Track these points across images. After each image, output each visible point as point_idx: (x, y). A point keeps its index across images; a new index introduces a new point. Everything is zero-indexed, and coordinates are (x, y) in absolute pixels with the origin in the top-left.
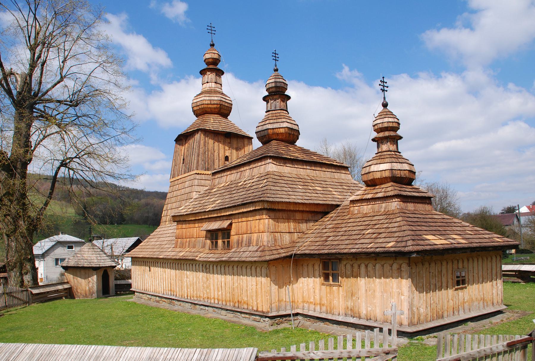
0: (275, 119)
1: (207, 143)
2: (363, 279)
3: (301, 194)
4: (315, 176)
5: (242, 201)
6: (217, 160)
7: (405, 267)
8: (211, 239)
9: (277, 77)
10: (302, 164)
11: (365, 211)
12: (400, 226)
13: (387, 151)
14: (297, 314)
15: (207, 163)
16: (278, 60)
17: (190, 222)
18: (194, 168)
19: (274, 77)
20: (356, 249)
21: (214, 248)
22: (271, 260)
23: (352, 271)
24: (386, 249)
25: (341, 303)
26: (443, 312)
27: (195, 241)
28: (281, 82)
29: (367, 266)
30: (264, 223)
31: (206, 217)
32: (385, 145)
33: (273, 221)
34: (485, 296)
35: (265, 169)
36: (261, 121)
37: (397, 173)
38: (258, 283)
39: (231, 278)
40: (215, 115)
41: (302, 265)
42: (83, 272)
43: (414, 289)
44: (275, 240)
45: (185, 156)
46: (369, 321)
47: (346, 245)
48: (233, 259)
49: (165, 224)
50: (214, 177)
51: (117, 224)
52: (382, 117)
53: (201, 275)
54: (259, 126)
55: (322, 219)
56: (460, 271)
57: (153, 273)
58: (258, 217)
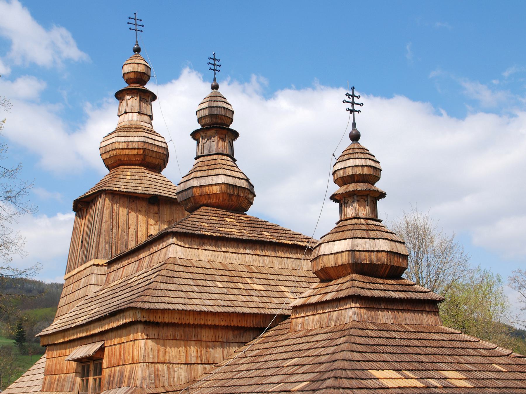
0: (205, 170)
1: (115, 214)
9: (214, 99)
10: (236, 245)
28: (220, 107)
31: (75, 337)
32: (351, 208)
33: (154, 344)
37: (362, 256)
40: (136, 167)
44: (157, 377)
45: (84, 236)
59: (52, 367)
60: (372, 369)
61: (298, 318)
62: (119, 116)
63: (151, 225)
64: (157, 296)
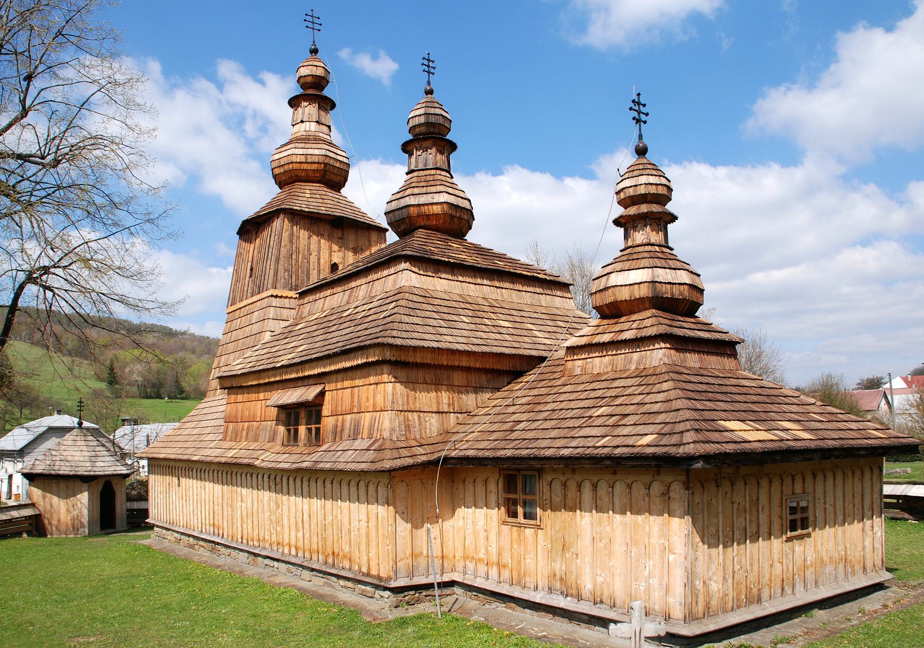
0: (423, 187)
1: (295, 238)
2: (587, 514)
3: (465, 333)
4: (500, 299)
5: (343, 346)
6: (316, 271)
7: (677, 490)
8: (287, 424)
11: (597, 368)
12: (668, 401)
13: (644, 245)
14: (452, 583)
15: (294, 276)
17: (250, 389)
18: (270, 286)
19: (424, 105)
20: (571, 450)
22: (395, 470)
23: (565, 496)
24: (636, 450)
25: (540, 564)
26: (759, 590)
28: (438, 115)
29: (596, 487)
30: (385, 391)
31: (278, 379)
32: (641, 232)
33: (403, 387)
34: (849, 553)
35: (395, 282)
36: (397, 190)
37: (664, 289)
38: (370, 516)
40: (315, 185)
41: (464, 482)
42: (62, 485)
43: (698, 539)
44: (408, 427)
45: (254, 263)
46: (598, 605)
47: (551, 440)
48: (321, 466)
49: (215, 395)
50: (301, 301)
51: (169, 399)
52: (635, 173)
53: (266, 496)
54: (391, 201)
55: (510, 386)
56: (797, 500)
57: (184, 490)
58: (372, 379)
59: (236, 413)
60: (720, 420)
61: (576, 360)
62: (293, 125)
63: (335, 252)
64: (405, 331)
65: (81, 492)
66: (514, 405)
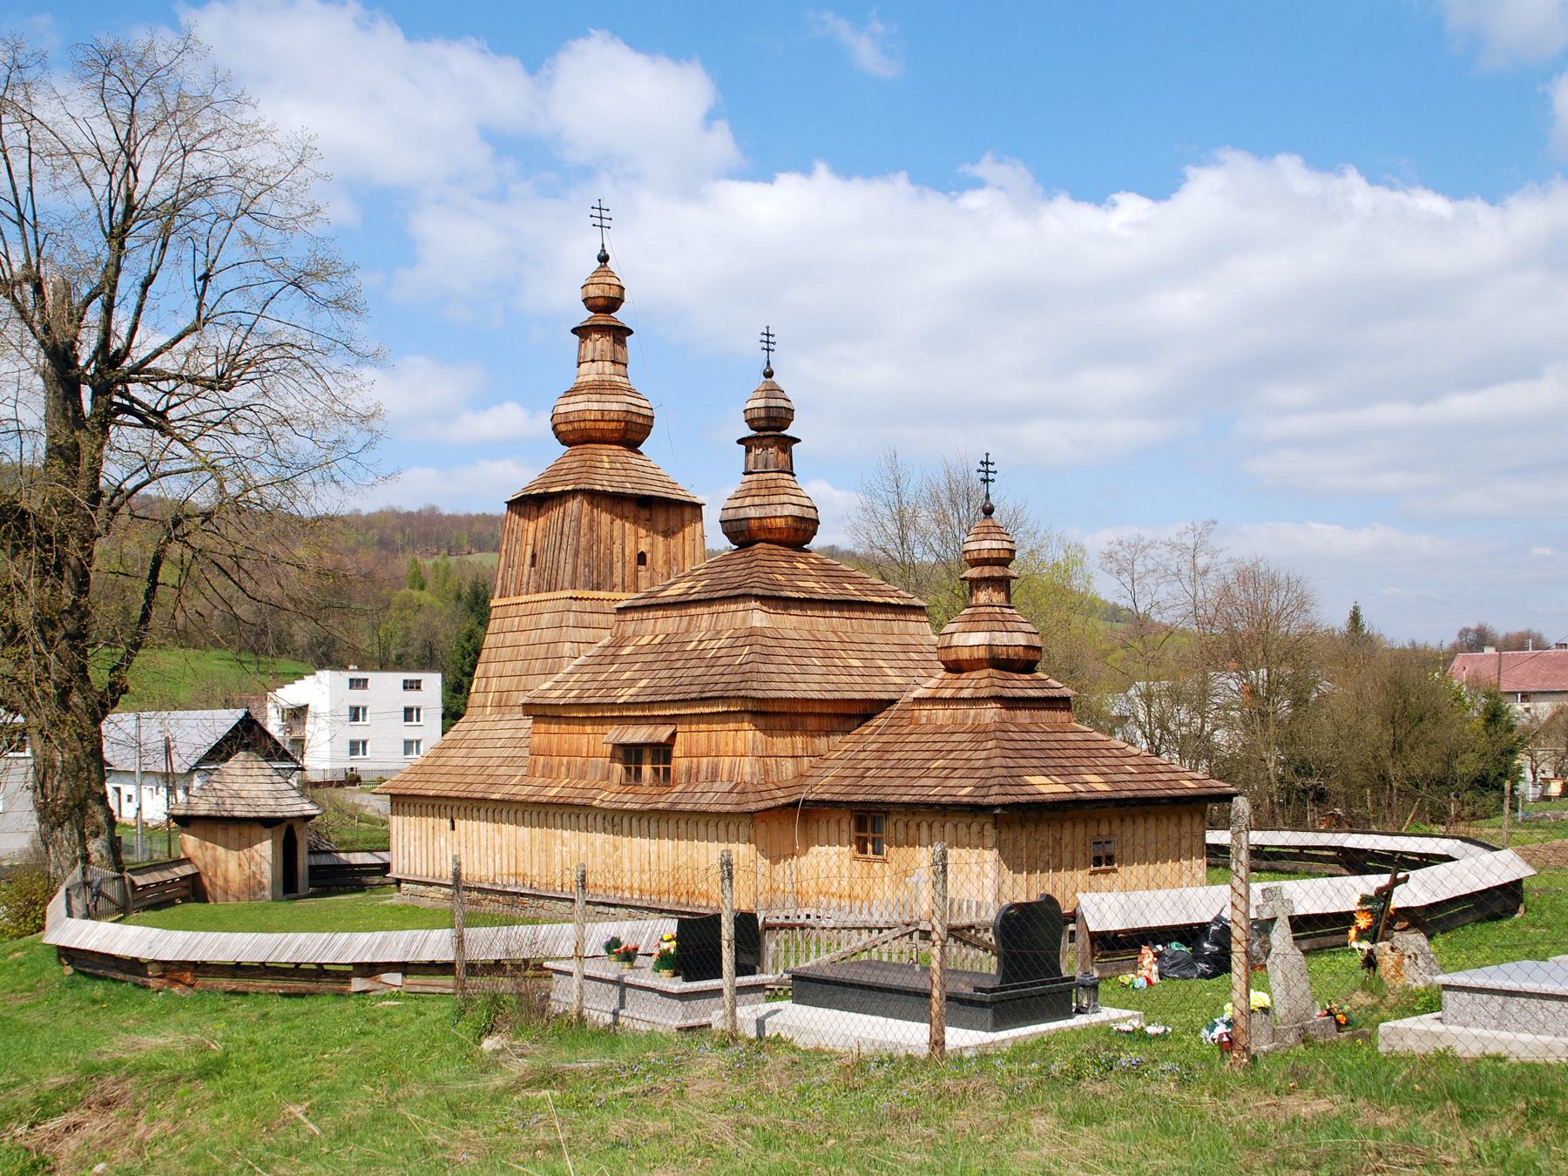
6: (620, 564)
7: (989, 830)
8: (626, 761)
9: (771, 394)
15: (595, 572)
16: (773, 350)
21: (633, 782)
24: (956, 799)
27: (584, 763)
35: (744, 620)
39: (673, 845)
42: (233, 832)
43: (1005, 867)
44: (767, 772)
48: (680, 807)
57: (462, 835)
58: (732, 726)
65: (261, 841)
66: (864, 751)
